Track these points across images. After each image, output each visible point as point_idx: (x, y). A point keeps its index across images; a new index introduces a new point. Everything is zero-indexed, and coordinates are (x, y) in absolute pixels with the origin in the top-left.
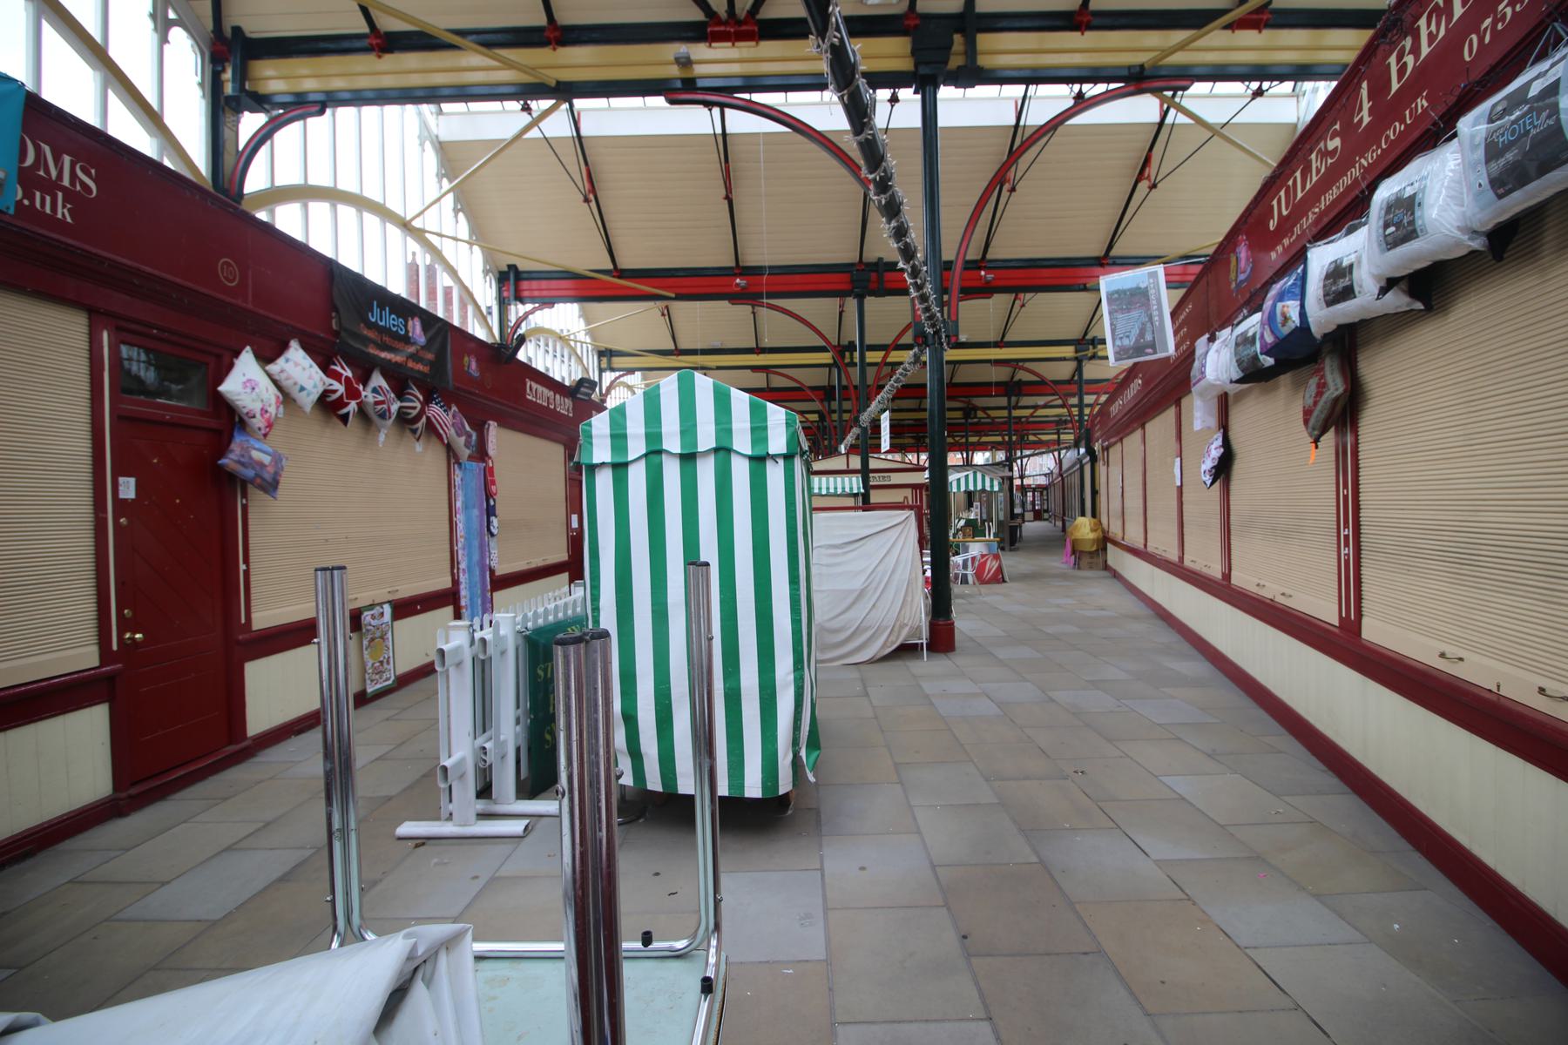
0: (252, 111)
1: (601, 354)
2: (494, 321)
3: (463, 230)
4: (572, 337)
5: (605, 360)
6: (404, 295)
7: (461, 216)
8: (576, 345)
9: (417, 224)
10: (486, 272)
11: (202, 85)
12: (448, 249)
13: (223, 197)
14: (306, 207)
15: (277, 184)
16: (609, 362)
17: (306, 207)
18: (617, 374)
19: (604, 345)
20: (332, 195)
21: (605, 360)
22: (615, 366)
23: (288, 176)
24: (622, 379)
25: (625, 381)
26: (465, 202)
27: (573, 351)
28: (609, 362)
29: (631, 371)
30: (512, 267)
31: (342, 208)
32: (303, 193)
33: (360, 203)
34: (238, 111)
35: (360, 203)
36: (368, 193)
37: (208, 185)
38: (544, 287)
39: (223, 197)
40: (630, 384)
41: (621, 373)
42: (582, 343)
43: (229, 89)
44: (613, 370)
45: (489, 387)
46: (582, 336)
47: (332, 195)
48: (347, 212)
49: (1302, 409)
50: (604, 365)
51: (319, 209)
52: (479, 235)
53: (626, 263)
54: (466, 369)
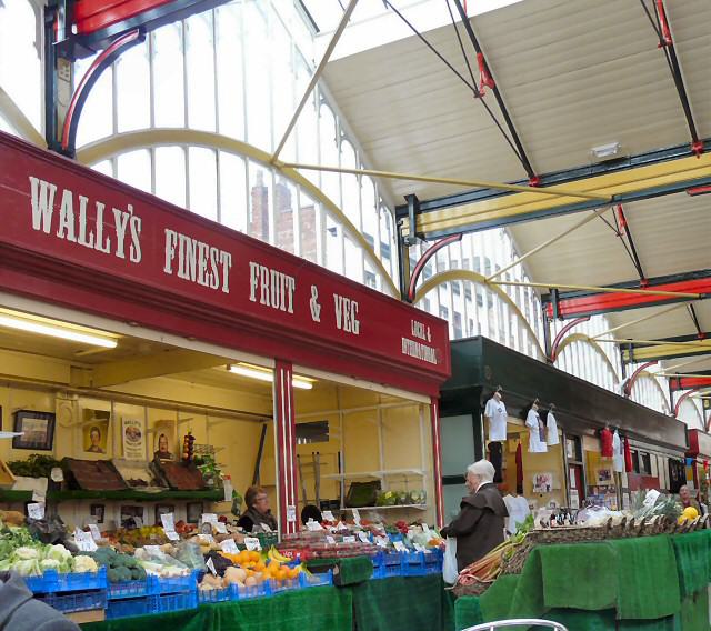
0: (82, 57)
1: (622, 347)
2: (392, 266)
3: (349, 158)
4: (503, 279)
5: (626, 352)
6: (245, 232)
7: (346, 145)
8: (509, 290)
9: (284, 158)
10: (379, 206)
11: (36, 45)
12: (329, 185)
13: (56, 154)
14: (152, 152)
15: (120, 132)
16: (632, 354)
17: (152, 152)
18: (639, 365)
19: (404, 189)
20: (184, 137)
21: (626, 352)
22: (636, 357)
23: (134, 120)
24: (572, 331)
25: (579, 332)
26: (353, 130)
27: (505, 298)
28: (632, 354)
29: (654, 361)
30: (412, 198)
31: (193, 150)
32: (151, 138)
33: (215, 142)
34: (71, 58)
35: (215, 142)
36: (225, 132)
37: (44, 146)
38: (573, 304)
39: (56, 154)
40: (591, 336)
41: (643, 364)
42: (517, 285)
43: (405, 233)
44: (635, 361)
45: (489, 378)
46: (517, 273)
47: (184, 137)
48: (201, 155)
49: (246, 489)
50: (626, 358)
51: (169, 154)
52: (370, 164)
53: (652, 272)
54: (168, 269)
